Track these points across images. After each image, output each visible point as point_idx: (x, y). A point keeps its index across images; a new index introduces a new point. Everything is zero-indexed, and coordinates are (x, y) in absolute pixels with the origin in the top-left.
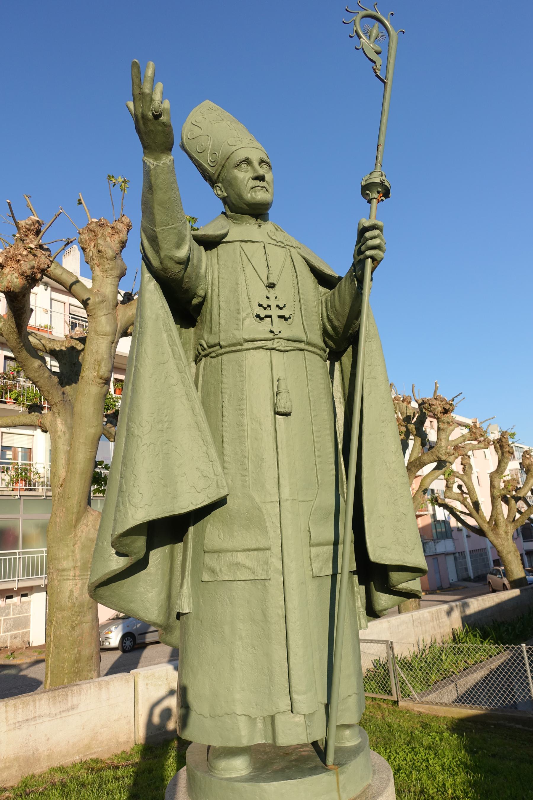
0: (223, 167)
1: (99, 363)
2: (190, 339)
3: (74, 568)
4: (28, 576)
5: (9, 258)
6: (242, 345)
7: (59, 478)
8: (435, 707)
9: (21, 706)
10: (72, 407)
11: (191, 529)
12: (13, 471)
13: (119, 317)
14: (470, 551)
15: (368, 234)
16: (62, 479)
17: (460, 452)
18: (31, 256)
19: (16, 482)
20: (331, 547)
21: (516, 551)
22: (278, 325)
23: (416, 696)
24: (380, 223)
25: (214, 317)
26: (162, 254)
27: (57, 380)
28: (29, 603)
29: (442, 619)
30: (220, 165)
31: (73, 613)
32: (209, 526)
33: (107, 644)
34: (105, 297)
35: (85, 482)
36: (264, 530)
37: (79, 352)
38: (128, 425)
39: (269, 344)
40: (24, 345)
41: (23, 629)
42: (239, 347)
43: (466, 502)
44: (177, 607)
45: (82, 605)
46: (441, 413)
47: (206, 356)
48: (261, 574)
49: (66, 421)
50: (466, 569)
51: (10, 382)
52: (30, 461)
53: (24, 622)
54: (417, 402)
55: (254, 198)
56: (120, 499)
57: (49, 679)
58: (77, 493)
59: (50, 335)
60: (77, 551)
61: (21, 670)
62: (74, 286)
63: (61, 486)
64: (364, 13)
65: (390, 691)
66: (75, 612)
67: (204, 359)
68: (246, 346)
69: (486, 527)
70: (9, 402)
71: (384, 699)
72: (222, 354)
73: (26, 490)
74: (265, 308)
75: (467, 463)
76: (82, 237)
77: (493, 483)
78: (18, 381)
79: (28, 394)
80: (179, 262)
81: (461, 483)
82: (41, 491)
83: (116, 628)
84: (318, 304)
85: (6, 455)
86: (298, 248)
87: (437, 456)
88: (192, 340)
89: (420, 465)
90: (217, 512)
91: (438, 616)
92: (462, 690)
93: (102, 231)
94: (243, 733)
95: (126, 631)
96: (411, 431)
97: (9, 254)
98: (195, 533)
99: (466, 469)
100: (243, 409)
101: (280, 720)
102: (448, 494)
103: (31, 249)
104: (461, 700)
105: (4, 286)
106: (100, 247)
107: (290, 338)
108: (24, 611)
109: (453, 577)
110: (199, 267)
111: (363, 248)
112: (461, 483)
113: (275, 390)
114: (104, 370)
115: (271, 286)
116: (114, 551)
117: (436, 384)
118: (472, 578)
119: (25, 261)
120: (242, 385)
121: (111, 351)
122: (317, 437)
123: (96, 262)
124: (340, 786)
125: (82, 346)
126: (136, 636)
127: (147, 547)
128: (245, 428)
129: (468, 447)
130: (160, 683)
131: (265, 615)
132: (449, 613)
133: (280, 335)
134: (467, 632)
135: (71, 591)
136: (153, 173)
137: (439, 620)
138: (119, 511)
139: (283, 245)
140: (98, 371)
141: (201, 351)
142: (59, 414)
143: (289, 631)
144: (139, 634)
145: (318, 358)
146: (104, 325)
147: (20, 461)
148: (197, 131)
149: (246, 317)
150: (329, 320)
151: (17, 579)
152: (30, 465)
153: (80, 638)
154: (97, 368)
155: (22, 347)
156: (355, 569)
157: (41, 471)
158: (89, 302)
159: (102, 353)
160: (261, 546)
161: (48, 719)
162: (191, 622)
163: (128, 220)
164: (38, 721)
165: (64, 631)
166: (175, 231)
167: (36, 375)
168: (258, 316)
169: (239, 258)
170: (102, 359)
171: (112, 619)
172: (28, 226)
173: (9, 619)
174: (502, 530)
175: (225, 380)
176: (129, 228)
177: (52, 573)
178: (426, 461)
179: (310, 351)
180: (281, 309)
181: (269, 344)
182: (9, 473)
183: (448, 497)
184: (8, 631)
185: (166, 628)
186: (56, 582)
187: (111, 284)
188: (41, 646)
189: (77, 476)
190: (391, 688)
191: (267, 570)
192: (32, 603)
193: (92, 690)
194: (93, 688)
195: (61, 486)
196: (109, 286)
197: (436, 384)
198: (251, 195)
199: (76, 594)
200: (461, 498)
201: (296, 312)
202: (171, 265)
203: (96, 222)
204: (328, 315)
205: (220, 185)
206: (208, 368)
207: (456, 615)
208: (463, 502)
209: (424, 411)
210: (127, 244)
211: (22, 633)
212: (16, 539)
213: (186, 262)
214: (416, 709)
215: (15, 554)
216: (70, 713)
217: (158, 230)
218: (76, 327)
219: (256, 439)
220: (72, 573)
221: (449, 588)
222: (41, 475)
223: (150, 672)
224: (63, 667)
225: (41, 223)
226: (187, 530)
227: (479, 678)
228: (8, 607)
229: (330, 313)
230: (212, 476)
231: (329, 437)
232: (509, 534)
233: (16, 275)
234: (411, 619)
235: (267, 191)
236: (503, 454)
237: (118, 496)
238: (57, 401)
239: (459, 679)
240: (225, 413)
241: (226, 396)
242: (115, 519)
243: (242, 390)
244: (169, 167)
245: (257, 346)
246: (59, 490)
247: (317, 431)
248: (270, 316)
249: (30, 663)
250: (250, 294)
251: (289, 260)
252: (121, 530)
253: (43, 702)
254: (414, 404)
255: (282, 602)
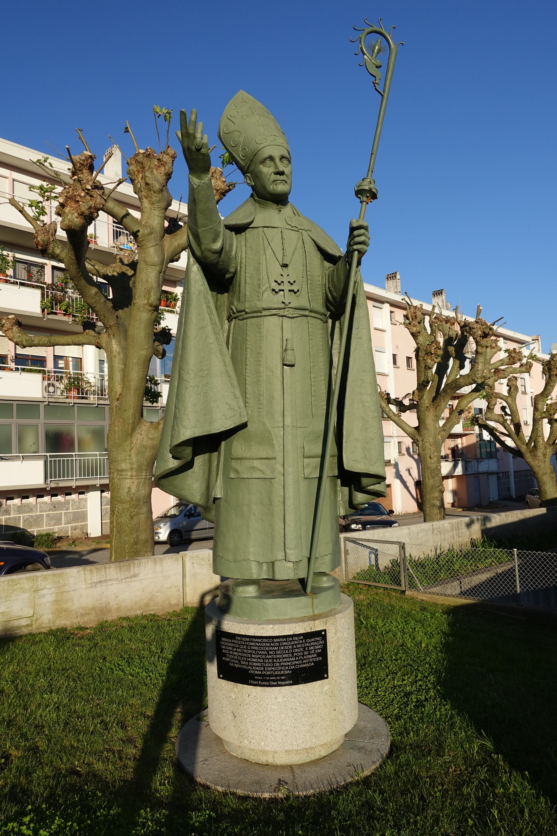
0: (251, 161)
1: (149, 292)
2: (224, 302)
3: (131, 469)
4: (84, 476)
5: (69, 198)
6: (261, 312)
7: (116, 392)
8: (436, 597)
9: (95, 571)
10: (126, 331)
11: (223, 443)
12: (66, 380)
13: (166, 248)
14: (515, 472)
15: (356, 233)
16: (118, 394)
17: (499, 375)
18: (88, 197)
19: (70, 390)
20: (320, 459)
21: (552, 472)
22: (289, 298)
23: (421, 587)
24: (365, 224)
25: (241, 289)
26: (203, 248)
27: (111, 305)
28: (86, 500)
29: (462, 529)
30: (249, 160)
31: (131, 505)
32: (235, 442)
33: (157, 538)
34: (153, 229)
35: (139, 397)
36: (272, 446)
37: (129, 278)
38: (179, 372)
39: (281, 312)
40: (82, 275)
41: (81, 522)
42: (259, 314)
43: (506, 424)
44: (213, 494)
45: (138, 500)
46: (480, 337)
47: (235, 318)
48: (269, 475)
49: (120, 342)
50: (509, 489)
51: (59, 293)
52: (81, 370)
53: (82, 516)
54: (459, 324)
55: (275, 190)
56: (175, 422)
57: (114, 556)
58: (132, 407)
59: (96, 245)
60: (133, 456)
61: (83, 555)
62: (125, 219)
63: (118, 400)
64: (370, 29)
65: (399, 583)
66: (133, 505)
67: (234, 320)
68: (264, 313)
69: (523, 448)
70: (60, 313)
71: (395, 589)
72: (247, 318)
73: (79, 398)
74: (279, 284)
75: (513, 385)
76: (130, 168)
77: (537, 406)
78: (66, 292)
79: (76, 305)
80: (215, 252)
81: (505, 404)
82: (92, 399)
83: (165, 525)
84: (322, 277)
85: (58, 364)
86: (309, 230)
87: (472, 380)
88: (226, 303)
89: (456, 387)
90: (240, 433)
91: (458, 527)
92: (465, 587)
93: (149, 163)
94: (254, 571)
95: (173, 528)
96: (450, 353)
97: (69, 194)
98: (225, 446)
99: (512, 390)
100: (260, 361)
101: (277, 564)
102: (489, 415)
103: (88, 190)
104: (463, 594)
105: (66, 224)
106: (148, 180)
107: (297, 307)
108: (82, 507)
109: (494, 495)
110: (231, 251)
111: (352, 242)
112: (505, 404)
113: (284, 348)
114: (153, 298)
115: (285, 266)
116: (171, 456)
117: (478, 307)
118: (514, 497)
119: (83, 202)
120: (261, 343)
121: (159, 281)
122: (314, 382)
123: (143, 193)
124: (314, 605)
125: (132, 272)
126: (183, 533)
127: (193, 454)
128: (262, 375)
129: (509, 370)
130: (204, 563)
131: (270, 501)
132: (469, 525)
133: (290, 306)
134: (484, 541)
135: (129, 488)
136: (196, 191)
137: (459, 530)
138: (175, 430)
139: (297, 229)
140: (148, 299)
141: (232, 314)
142: (113, 336)
143: (286, 512)
144: (186, 532)
145: (319, 321)
146: (153, 256)
147: (71, 370)
148: (232, 127)
149: (265, 291)
150: (330, 291)
151: (74, 478)
152: (81, 374)
153: (137, 525)
154: (147, 297)
155: (80, 276)
156: (337, 474)
157: (92, 380)
158: (139, 234)
159: (151, 283)
160: (270, 457)
161: (116, 582)
162: (222, 504)
163: (173, 152)
164: (108, 583)
165: (124, 519)
166: (212, 230)
167: (94, 300)
168: (274, 290)
169: (261, 241)
170: (151, 288)
171: (161, 517)
172: (82, 162)
173: (69, 513)
174: (540, 453)
175: (248, 338)
176: (174, 157)
177: (113, 472)
178: (462, 384)
179: (313, 317)
180: (292, 284)
181: (281, 312)
182: (63, 381)
183: (488, 420)
184: (69, 523)
185: (207, 509)
186: (116, 480)
187: (158, 216)
188: (98, 537)
189: (132, 392)
190: (400, 581)
191: (273, 472)
192: (88, 500)
193: (149, 564)
194: (150, 562)
195: (118, 400)
196: (156, 218)
197: (478, 307)
198: (273, 187)
199: (133, 490)
200: (501, 420)
201: (304, 286)
202: (209, 254)
203: (143, 154)
204: (329, 288)
205: (249, 175)
206: (237, 328)
207: (477, 528)
208: (503, 423)
209: (465, 333)
210: (172, 175)
211: (81, 525)
212: (72, 442)
213: (220, 252)
214: (419, 597)
215: (72, 456)
216: (133, 579)
217: (199, 230)
218: (120, 235)
219: (269, 383)
220: (129, 473)
221: (488, 505)
222: (92, 384)
223: (195, 554)
224: (124, 548)
225: (93, 157)
226: (220, 444)
227: (485, 578)
228: (67, 502)
229: (331, 286)
230: (237, 409)
231: (323, 382)
232: (547, 456)
233: (76, 214)
234: (431, 528)
235: (286, 182)
236: (550, 376)
237: (174, 420)
238: (111, 324)
239: (464, 578)
240: (248, 363)
241: (249, 350)
242: (172, 435)
243: (260, 347)
244: (207, 184)
245: (272, 313)
246: (116, 403)
247: (314, 378)
248: (283, 290)
249: (89, 550)
250: (269, 272)
251: (301, 242)
252: (176, 442)
253: (112, 570)
254: (457, 328)
255: (282, 493)
